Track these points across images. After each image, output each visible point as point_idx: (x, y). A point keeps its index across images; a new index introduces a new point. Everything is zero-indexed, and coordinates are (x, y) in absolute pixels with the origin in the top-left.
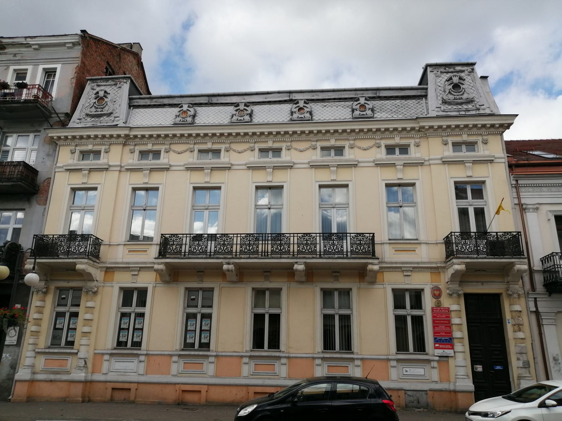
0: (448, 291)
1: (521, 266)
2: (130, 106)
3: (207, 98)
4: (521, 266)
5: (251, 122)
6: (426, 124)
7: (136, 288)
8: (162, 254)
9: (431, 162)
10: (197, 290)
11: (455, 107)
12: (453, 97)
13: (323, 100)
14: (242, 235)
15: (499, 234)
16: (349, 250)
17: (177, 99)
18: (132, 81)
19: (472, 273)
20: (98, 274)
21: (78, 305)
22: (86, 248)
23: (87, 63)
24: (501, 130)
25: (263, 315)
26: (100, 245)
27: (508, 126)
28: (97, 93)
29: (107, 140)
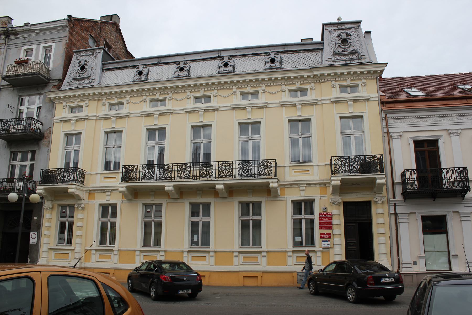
0: (330, 201)
1: (380, 179)
2: (103, 70)
3: (157, 59)
4: (380, 179)
5: (188, 76)
6: (319, 72)
7: (110, 205)
8: (125, 178)
9: (323, 102)
11: (343, 58)
12: (342, 50)
13: (244, 55)
15: (366, 157)
16: (256, 173)
17: (136, 62)
18: (104, 50)
19: (345, 187)
20: (84, 195)
21: (73, 217)
22: (74, 177)
23: (73, 39)
26: (84, 174)
28: (80, 62)
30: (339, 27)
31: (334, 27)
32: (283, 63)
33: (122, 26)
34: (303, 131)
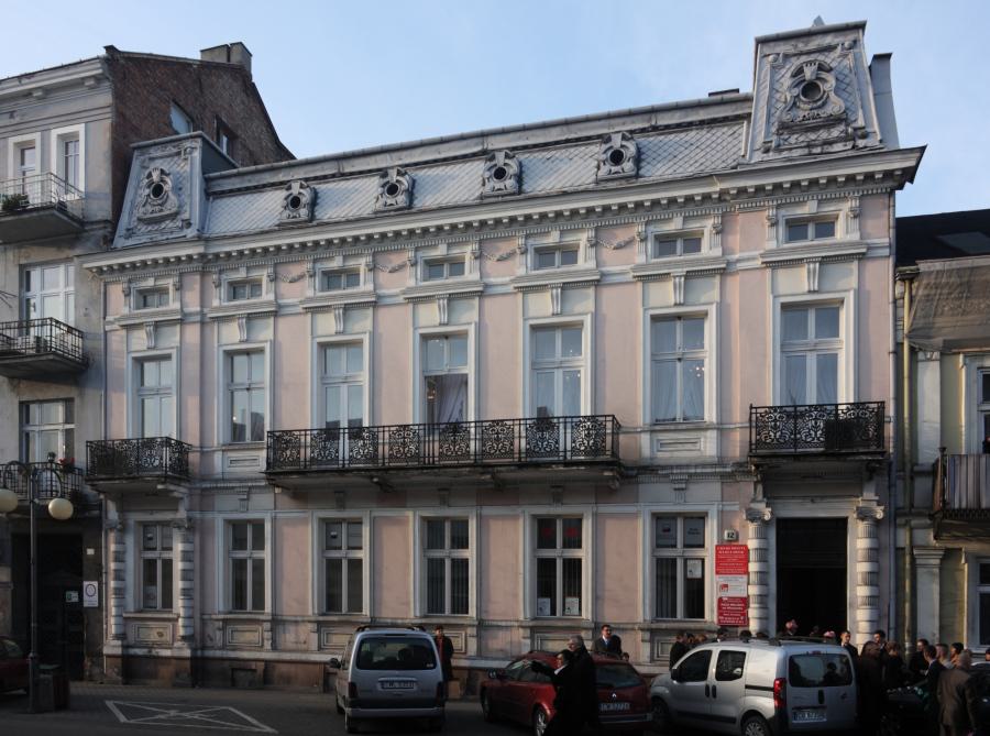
3: (334, 164)
10: (339, 522)
14: (392, 429)
15: (840, 407)
16: (569, 448)
18: (204, 140)
23: (128, 113)
24: (889, 184)
25: (442, 561)
27: (909, 175)
29: (186, 266)
30: (801, 46)
31: (783, 48)
32: (643, 164)
33: (258, 78)
34: (686, 344)
